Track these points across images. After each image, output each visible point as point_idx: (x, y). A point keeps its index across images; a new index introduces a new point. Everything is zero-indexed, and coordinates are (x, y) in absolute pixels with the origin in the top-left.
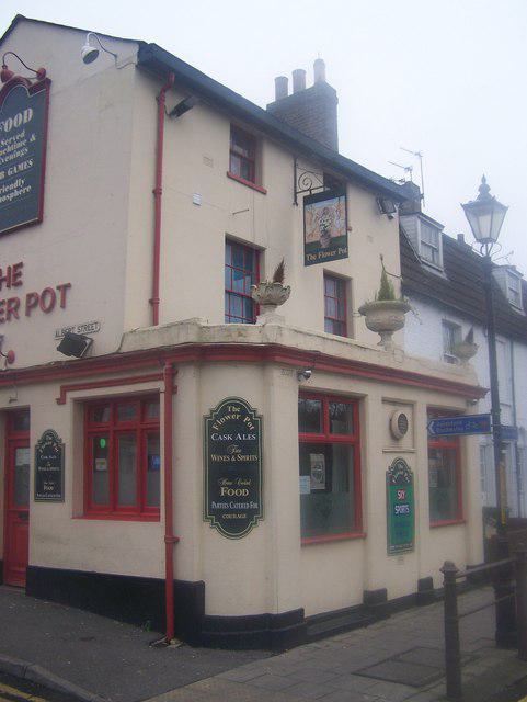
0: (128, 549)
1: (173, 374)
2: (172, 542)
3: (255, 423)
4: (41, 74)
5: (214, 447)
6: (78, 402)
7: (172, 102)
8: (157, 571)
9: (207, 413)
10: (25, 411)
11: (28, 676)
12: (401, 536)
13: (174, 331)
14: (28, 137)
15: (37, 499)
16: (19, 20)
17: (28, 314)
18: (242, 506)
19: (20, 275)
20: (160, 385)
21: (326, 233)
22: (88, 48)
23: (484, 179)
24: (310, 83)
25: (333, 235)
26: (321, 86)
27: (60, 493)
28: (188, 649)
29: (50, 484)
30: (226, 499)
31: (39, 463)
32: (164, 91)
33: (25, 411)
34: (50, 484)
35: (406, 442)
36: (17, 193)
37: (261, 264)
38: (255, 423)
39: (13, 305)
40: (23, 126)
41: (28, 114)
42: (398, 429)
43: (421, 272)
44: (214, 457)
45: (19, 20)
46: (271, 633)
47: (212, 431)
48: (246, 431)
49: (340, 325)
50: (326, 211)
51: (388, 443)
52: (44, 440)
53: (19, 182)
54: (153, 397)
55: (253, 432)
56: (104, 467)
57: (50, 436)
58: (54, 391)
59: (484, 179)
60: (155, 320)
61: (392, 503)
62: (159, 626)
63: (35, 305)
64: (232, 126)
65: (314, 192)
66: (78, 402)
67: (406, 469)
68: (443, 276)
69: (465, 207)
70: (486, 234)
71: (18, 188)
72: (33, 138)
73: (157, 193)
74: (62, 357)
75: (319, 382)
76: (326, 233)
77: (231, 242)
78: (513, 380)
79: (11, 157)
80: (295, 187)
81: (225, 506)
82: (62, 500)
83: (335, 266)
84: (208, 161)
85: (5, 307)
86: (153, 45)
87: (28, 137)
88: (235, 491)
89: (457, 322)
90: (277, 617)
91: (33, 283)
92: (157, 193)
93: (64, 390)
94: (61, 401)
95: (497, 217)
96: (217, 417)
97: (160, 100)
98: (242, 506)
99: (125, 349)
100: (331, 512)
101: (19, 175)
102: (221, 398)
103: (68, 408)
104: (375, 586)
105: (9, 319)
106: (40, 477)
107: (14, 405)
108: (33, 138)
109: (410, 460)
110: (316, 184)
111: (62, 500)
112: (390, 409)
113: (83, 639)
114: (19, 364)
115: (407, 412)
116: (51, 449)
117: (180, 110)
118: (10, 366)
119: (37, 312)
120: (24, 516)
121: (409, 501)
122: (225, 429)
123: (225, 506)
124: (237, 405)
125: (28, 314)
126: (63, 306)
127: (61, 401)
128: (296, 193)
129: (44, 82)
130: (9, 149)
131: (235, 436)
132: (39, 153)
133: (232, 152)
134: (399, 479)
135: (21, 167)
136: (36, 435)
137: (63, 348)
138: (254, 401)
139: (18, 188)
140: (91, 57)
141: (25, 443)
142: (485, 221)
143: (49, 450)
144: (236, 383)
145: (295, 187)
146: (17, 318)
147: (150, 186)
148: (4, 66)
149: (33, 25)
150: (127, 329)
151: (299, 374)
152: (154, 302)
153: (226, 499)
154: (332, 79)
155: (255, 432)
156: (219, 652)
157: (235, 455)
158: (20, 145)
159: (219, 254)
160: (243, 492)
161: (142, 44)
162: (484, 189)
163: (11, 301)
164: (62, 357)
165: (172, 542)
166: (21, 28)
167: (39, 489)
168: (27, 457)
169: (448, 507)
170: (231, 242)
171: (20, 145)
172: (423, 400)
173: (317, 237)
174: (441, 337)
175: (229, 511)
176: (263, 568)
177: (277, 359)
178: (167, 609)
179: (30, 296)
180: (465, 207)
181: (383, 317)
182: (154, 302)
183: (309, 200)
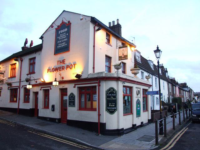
0: (90, 117)
1: (100, 82)
2: (99, 115)
3: (115, 92)
4: (69, 22)
5: (107, 97)
7: (97, 28)
8: (96, 121)
9: (106, 90)
10: (66, 89)
11: (75, 141)
12: (138, 115)
13: (100, 74)
14: (66, 34)
15: (69, 106)
16: (64, 11)
18: (113, 108)
19: (65, 61)
20: (97, 85)
21: (123, 54)
22: (81, 18)
23: (158, 46)
24: (116, 24)
25: (125, 55)
27: (116, 107)
28: (103, 136)
29: (72, 103)
30: (110, 107)
31: (69, 99)
32: (95, 26)
33: (66, 89)
34: (72, 103)
35: (139, 95)
36: (64, 45)
38: (115, 92)
39: (63, 68)
40: (65, 32)
41: (66, 30)
42: (138, 93)
43: (137, 62)
44: (108, 99)
45: (64, 11)
46: (119, 133)
47: (107, 94)
48: (114, 94)
49: (109, 70)
50: (123, 50)
51: (137, 97)
52: (71, 95)
53: (64, 43)
54: (95, 87)
55: (116, 94)
56: (83, 100)
57: (72, 94)
58: (73, 85)
59: (158, 46)
60: (94, 72)
61: (137, 107)
62: (97, 132)
64: (106, 33)
66: (78, 87)
67: (139, 101)
68: (140, 62)
69: (154, 51)
70: (158, 56)
71: (64, 44)
72: (67, 34)
73: (94, 46)
74: (76, 78)
75: (127, 84)
76: (123, 54)
77: (106, 56)
79: (62, 38)
81: (110, 108)
82: (75, 107)
83: (124, 61)
85: (61, 68)
86: (94, 17)
87: (66, 34)
89: (143, 71)
90: (120, 129)
91: (67, 62)
92: (94, 46)
93: (75, 85)
94: (75, 87)
95: (160, 53)
96: (109, 91)
97: (94, 28)
98: (113, 108)
99: (89, 77)
100: (128, 110)
101: (64, 42)
102: (109, 88)
103: (76, 88)
104: (134, 124)
106: (70, 102)
107: (64, 87)
108: (67, 34)
109: (140, 99)
110: (120, 44)
111: (75, 107)
112: (136, 89)
113: (83, 134)
114: (64, 79)
115: (139, 89)
116: (72, 96)
117: (98, 30)
118: (63, 80)
120: (66, 110)
121: (140, 107)
122: (110, 93)
123: (110, 108)
124: (112, 89)
127: (75, 87)
128: (117, 46)
129: (69, 23)
130: (62, 36)
132: (68, 37)
133: (106, 38)
134: (138, 103)
135: (65, 40)
136: (69, 94)
137: (76, 77)
138: (116, 88)
139: (64, 44)
140: (81, 19)
141: (66, 95)
142: (158, 54)
143: (72, 97)
146: (64, 70)
147: (95, 47)
148: (63, 20)
149: (77, 14)
150: (89, 73)
151: (123, 83)
152: (94, 68)
153: (110, 107)
154: (120, 23)
155: (116, 94)
157: (112, 98)
158: (64, 36)
159: (104, 58)
160: (114, 106)
161: (92, 17)
162: (158, 48)
163: (63, 67)
164: (76, 78)
165: (99, 115)
166: (64, 12)
167: (70, 104)
168: (66, 98)
169: (146, 109)
170: (106, 56)
171: (64, 36)
172: (142, 87)
173: (121, 55)
175: (111, 109)
176: (118, 120)
177: (120, 80)
178: (98, 128)
180: (154, 51)
181: (135, 71)
182: (94, 68)
183: (120, 48)
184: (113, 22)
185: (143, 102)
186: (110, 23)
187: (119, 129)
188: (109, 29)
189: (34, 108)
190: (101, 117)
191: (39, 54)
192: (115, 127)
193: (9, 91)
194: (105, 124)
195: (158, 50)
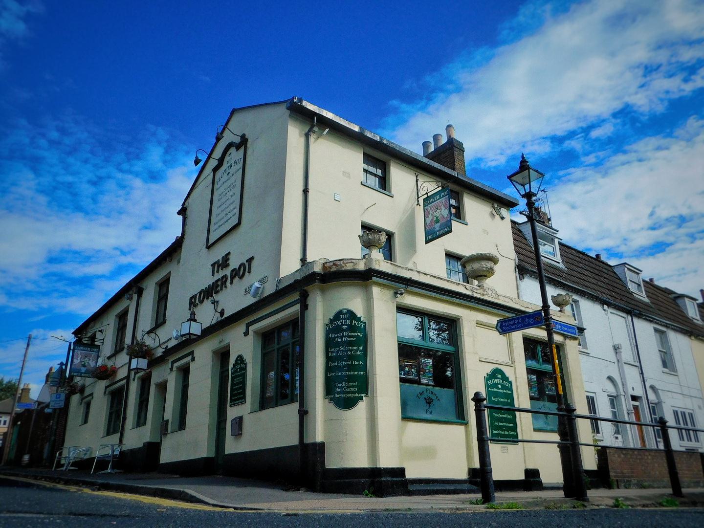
6: (256, 332)
17: (231, 283)
24: (443, 140)
26: (451, 141)
37: (392, 244)
52: (237, 360)
63: (235, 276)
64: (365, 154)
65: (429, 194)
66: (256, 332)
73: (306, 191)
78: (637, 346)
80: (418, 193)
84: (346, 174)
88: (349, 383)
92: (306, 191)
105: (221, 289)
119: (237, 279)
125: (231, 283)
126: (249, 272)
127: (246, 334)
131: (349, 341)
144: (352, 300)
145: (418, 193)
147: (310, 195)
151: (396, 293)
154: (456, 136)
156: (161, 327)
163: (223, 277)
165: (303, 414)
174: (323, 140)
178: (302, 467)
179: (232, 271)
184: (436, 137)
185: (527, 358)
186: (425, 145)
187: (378, 466)
188: (426, 161)
189: (213, 455)
190: (308, 419)
191: (179, 262)
192: (359, 460)
193: (106, 399)
194: (322, 445)
195: (449, 126)
